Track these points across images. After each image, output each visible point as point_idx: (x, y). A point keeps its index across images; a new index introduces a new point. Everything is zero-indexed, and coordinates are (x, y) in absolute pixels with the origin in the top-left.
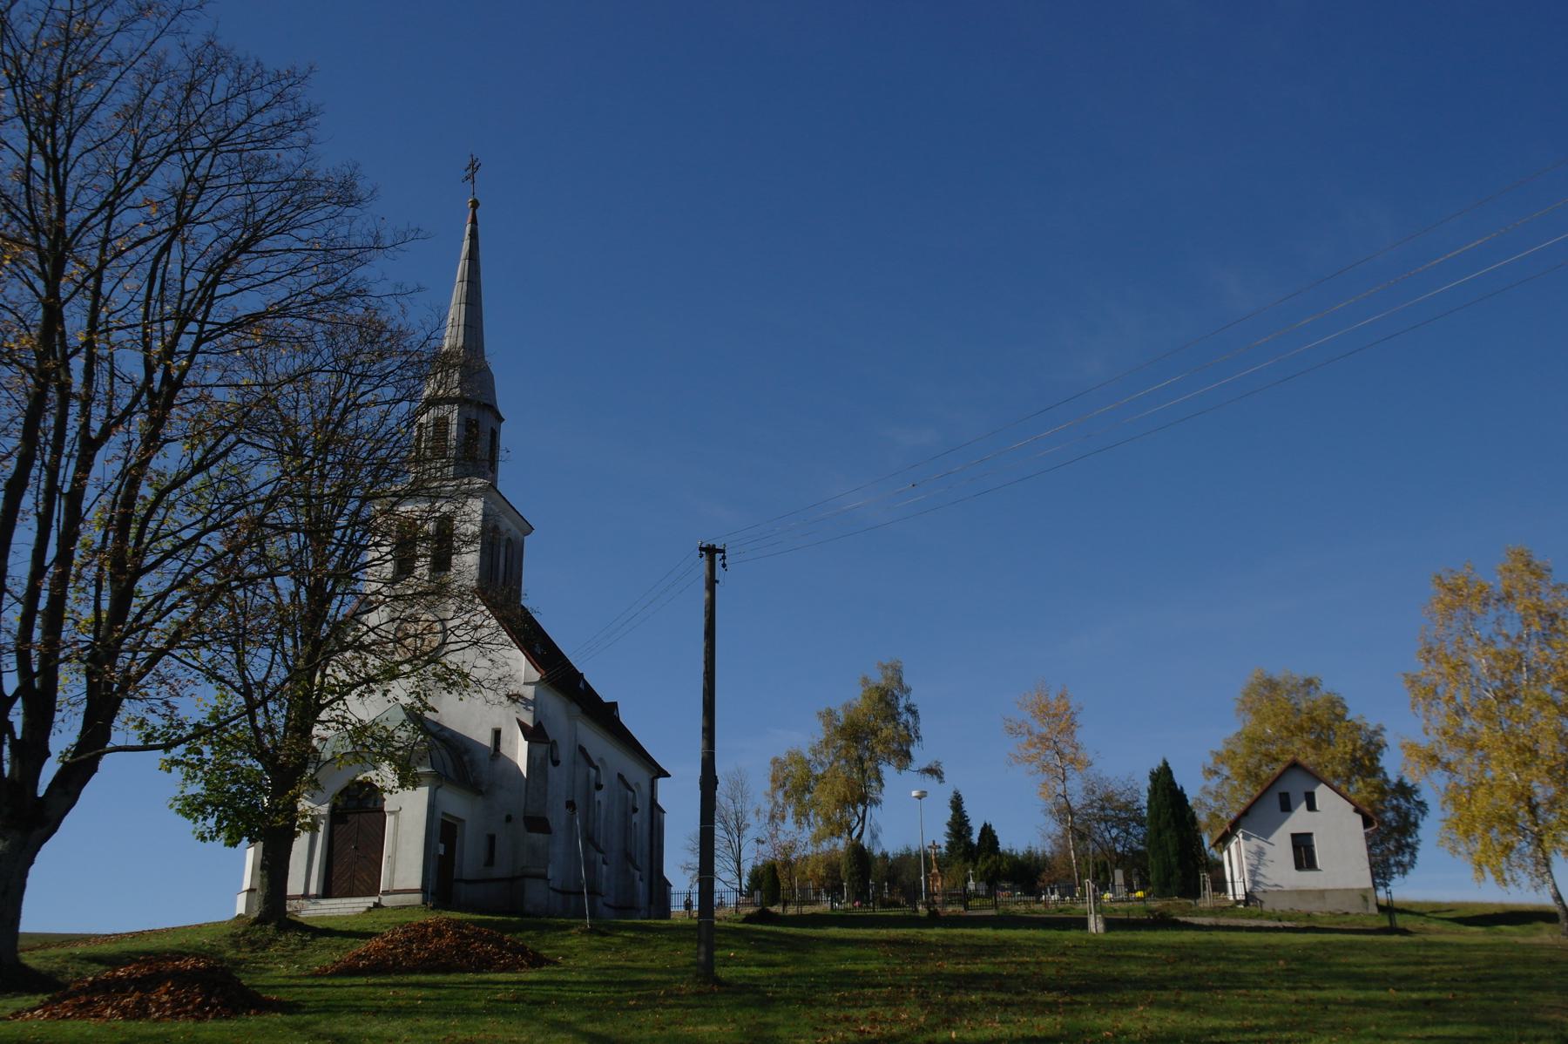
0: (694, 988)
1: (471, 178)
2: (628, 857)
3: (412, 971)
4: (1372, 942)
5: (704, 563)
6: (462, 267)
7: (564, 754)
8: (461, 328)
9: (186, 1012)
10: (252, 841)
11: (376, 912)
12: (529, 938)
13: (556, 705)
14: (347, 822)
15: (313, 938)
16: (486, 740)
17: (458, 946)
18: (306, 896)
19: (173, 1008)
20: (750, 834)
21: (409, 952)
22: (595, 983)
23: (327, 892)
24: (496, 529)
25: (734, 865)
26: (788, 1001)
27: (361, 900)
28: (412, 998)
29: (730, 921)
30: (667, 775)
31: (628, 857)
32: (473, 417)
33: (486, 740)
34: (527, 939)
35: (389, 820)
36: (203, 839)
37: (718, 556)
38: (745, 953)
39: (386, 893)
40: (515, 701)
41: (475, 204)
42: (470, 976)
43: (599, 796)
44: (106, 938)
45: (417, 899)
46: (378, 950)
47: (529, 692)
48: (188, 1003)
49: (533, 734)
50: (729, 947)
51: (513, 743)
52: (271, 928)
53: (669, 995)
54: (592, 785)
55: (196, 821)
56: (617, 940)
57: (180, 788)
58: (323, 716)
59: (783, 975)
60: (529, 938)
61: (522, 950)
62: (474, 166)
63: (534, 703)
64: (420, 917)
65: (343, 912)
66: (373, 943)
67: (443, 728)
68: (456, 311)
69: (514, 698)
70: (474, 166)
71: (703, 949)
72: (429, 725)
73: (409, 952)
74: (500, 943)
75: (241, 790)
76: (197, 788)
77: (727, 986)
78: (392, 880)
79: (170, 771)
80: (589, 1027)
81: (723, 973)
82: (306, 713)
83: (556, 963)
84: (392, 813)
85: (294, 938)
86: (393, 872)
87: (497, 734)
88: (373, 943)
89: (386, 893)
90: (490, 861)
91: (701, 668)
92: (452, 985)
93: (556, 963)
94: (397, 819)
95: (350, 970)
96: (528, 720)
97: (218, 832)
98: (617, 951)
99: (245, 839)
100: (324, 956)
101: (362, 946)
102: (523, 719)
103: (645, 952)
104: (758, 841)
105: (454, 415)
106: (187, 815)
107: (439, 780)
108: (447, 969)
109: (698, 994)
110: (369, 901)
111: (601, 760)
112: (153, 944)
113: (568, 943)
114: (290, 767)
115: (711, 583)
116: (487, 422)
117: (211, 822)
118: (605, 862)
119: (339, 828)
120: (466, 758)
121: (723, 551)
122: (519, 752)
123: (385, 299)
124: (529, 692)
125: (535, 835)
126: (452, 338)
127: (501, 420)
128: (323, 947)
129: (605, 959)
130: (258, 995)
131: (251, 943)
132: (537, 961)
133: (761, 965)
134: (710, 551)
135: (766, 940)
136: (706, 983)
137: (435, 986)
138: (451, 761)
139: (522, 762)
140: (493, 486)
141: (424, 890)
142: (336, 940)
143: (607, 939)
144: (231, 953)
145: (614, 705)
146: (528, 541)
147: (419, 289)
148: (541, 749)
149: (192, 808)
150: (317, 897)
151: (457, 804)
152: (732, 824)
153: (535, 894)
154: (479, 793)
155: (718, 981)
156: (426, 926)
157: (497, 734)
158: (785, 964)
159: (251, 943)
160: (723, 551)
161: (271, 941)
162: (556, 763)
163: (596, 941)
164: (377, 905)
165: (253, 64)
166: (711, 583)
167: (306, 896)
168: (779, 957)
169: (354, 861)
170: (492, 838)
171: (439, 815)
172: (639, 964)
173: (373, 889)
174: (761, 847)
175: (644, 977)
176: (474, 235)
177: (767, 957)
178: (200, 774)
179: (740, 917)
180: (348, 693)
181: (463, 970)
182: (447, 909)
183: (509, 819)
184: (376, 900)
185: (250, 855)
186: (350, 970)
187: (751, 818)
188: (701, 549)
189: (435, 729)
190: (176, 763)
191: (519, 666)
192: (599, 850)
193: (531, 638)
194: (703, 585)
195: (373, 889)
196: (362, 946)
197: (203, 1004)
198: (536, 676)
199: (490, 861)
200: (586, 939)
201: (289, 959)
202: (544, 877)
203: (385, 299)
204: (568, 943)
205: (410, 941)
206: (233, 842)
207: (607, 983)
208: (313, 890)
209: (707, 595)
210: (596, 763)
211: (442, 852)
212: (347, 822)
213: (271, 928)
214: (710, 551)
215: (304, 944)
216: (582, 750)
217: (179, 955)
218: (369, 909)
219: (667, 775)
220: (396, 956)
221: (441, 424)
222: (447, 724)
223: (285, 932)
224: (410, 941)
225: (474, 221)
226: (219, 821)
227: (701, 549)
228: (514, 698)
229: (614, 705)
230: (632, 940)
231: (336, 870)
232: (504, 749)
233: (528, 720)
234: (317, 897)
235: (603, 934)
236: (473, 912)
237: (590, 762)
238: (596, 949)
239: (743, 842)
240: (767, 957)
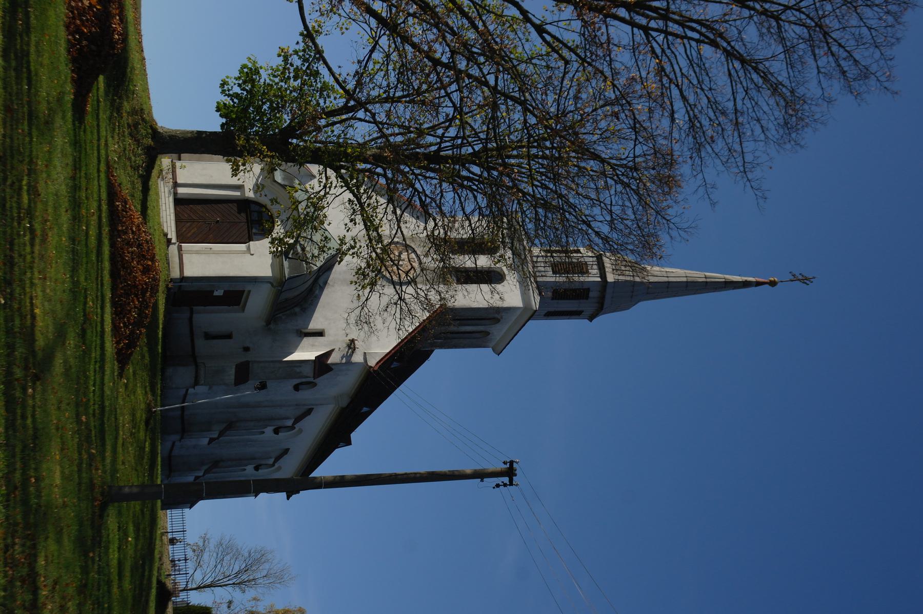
0: (97, 481)
1: (795, 279)
2: (216, 464)
3: (113, 245)
4: (158, 327)
5: (500, 467)
6: (719, 276)
7: (306, 395)
8: (666, 279)
9: (74, 18)
10: (222, 126)
11: (164, 240)
12: (143, 357)
13: (347, 383)
14: (239, 213)
15: (140, 176)
16: (315, 324)
17: (135, 286)
18: (176, 185)
19: (77, 8)
20: (236, 595)
21: (129, 244)
22: (103, 402)
23: (179, 202)
24: (497, 321)
25: (208, 582)
26: (85, 570)
27: (174, 229)
28: (95, 371)
29: (159, 569)
30: (288, 499)
31: (216, 464)
32: (591, 294)
33: (315, 324)
34: (141, 352)
35: (242, 247)
36: (222, 85)
37: (506, 480)
38: (130, 551)
39: (180, 249)
40: (349, 346)
41: (773, 284)
42: (108, 295)
43: (269, 431)
44: (139, 33)
45: (175, 274)
46: (131, 218)
47: (358, 358)
48: (81, 20)
49: (321, 364)
50: (137, 539)
51: (313, 347)
52: (150, 142)
53: (91, 457)
54: (279, 423)
55: (236, 79)
56: (142, 434)
57: (264, 65)
58: (330, 172)
59: (109, 583)
60: (143, 357)
61: (132, 345)
62: (805, 280)
63: (349, 362)
64: (162, 277)
65: (163, 214)
66: (138, 219)
67: (322, 289)
68: (678, 274)
69: (352, 345)
70: (805, 280)
71: (135, 490)
72: (324, 277)
73: (129, 244)
74: (138, 324)
75: (264, 114)
76: (264, 77)
77: (97, 521)
78: (190, 252)
79: (279, 56)
80: (58, 361)
81: (112, 511)
82: (335, 157)
83: (121, 375)
84: (249, 248)
85: (140, 160)
86: (197, 252)
87: (320, 334)
88: (138, 219)
89: (180, 249)
90: (208, 336)
91: (400, 470)
92: (100, 270)
93: (121, 375)
94: (243, 253)
95: (113, 193)
96: (333, 359)
97: (229, 95)
98: (132, 434)
99: (224, 120)
100: (126, 180)
101: (135, 207)
102: (333, 355)
103: (131, 459)
104: (230, 602)
105: (593, 276)
106: (241, 72)
107: (279, 284)
108: (114, 275)
109: (92, 486)
110: (172, 235)
111: (301, 431)
112: (134, 56)
113: (139, 391)
114: (283, 147)
115: (480, 475)
116: (587, 306)
117: (237, 90)
118: (211, 440)
119: (234, 207)
120: (297, 309)
121: (511, 484)
122: (305, 353)
123: (700, 176)
124: (358, 358)
125: (233, 371)
126: (657, 272)
127: (591, 319)
128: (133, 183)
129: (125, 419)
130: (89, 91)
131: (136, 125)
132: (123, 358)
133: (120, 564)
134: (510, 472)
135: (143, 575)
136: (102, 494)
137: (99, 253)
138: (295, 297)
139: (296, 356)
140: (534, 315)
141: (183, 279)
142: (139, 195)
143: (142, 426)
144: (127, 106)
145: (349, 443)
146: (486, 353)
147: (713, 204)
148: (308, 371)
149: (249, 75)
150: (175, 194)
151: (258, 303)
152: (244, 577)
153: (182, 375)
154: (268, 323)
155: (103, 507)
156: (153, 259)
157: (320, 334)
158: (120, 587)
159: (136, 125)
160: (511, 484)
161: (138, 142)
162: (297, 388)
163: (141, 415)
164: (169, 242)
165: (899, 35)
166: (480, 475)
167: (176, 185)
168: (127, 585)
169: (209, 218)
170: (229, 336)
171: (248, 287)
172: (120, 449)
173: (183, 237)
174: (225, 606)
175: (109, 448)
176: (746, 284)
177: (127, 573)
178: (277, 80)
179: (163, 578)
180: (352, 192)
181: (114, 289)
182: (167, 299)
183: (247, 349)
184: (174, 240)
185: (213, 123)
186: (113, 193)
187: (251, 593)
188: (512, 463)
189: (321, 282)
190: (286, 59)
191: (380, 344)
192: (221, 434)
193: (406, 359)
194: (478, 468)
195: (183, 237)
196: (135, 207)
197: (82, 34)
198: (372, 362)
199: (208, 336)
200: (143, 406)
201: (123, 154)
202: (196, 383)
203: (700, 176)
204: (139, 391)
205: (139, 246)
206: (221, 109)
207: (102, 407)
208: (181, 190)
209: (469, 471)
210: (297, 426)
211: (216, 293)
212: (239, 213)
213: (150, 142)
214: (510, 472)
215: (135, 168)
216: (309, 412)
217: (123, 20)
218: (166, 235)
219: (288, 499)
220: (126, 233)
221: (582, 268)
222: (325, 292)
223: (145, 154)
224: (139, 246)
225: (758, 284)
226: (237, 95)
227: (512, 463)
228: (352, 345)
229: (349, 443)
230: (142, 448)
231: (199, 207)
232: (307, 341)
233: (333, 359)
234: (175, 194)
235: (147, 423)
236: (163, 334)
237: (298, 419)
238: (134, 415)
239: (230, 588)
240: (127, 573)
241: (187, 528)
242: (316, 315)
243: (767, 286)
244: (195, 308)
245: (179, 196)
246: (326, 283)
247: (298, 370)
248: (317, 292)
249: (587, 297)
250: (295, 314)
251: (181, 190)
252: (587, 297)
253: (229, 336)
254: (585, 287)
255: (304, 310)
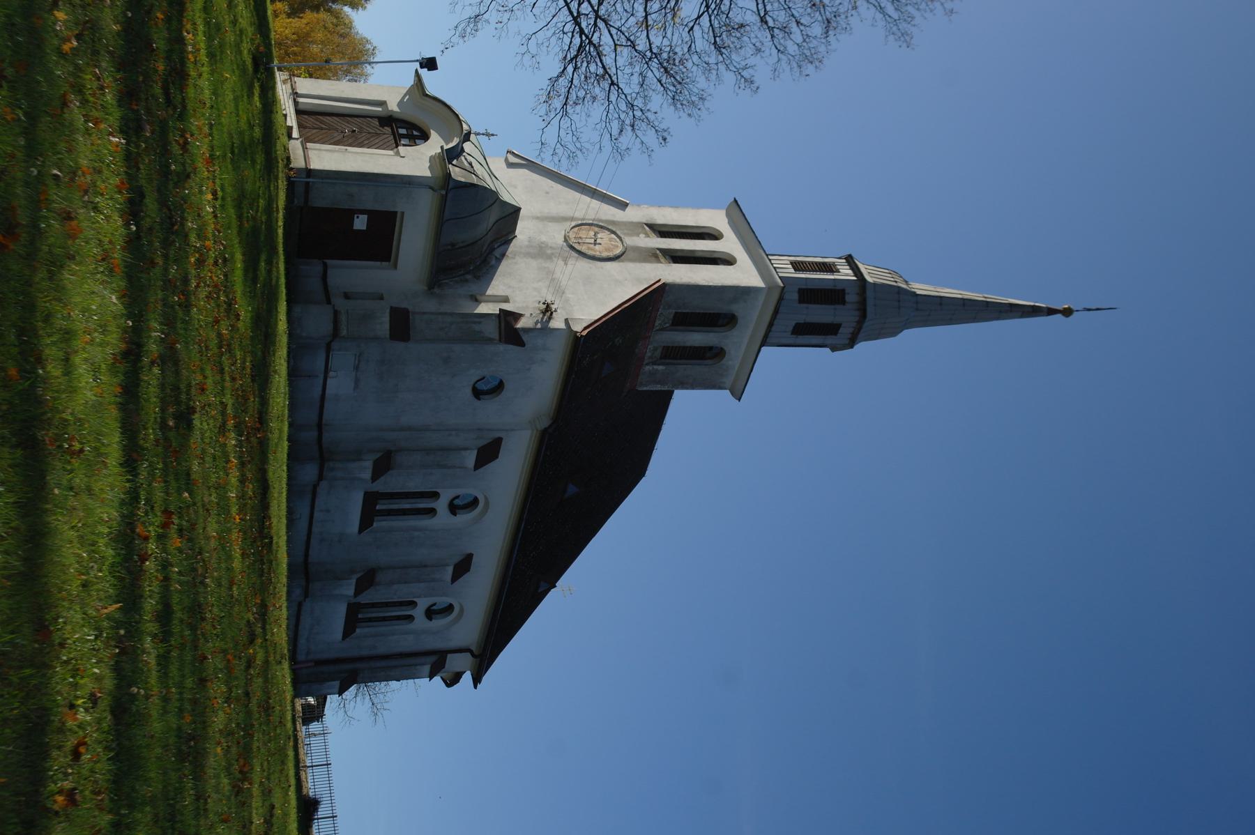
30: (475, 687)
32: (848, 298)
41: (1067, 312)
47: (557, 323)
67: (499, 261)
69: (548, 310)
120: (468, 277)
124: (557, 323)
195: (306, 139)
199: (347, 296)
219: (475, 687)
228: (548, 310)
241: (338, 812)
242: (493, 282)
243: (1059, 316)
244: (329, 262)
245: (301, 107)
246: (503, 255)
247: (477, 328)
248: (493, 262)
249: (843, 302)
250: (467, 281)
251: (301, 100)
252: (843, 302)
253: (382, 298)
254: (839, 287)
255: (478, 278)
